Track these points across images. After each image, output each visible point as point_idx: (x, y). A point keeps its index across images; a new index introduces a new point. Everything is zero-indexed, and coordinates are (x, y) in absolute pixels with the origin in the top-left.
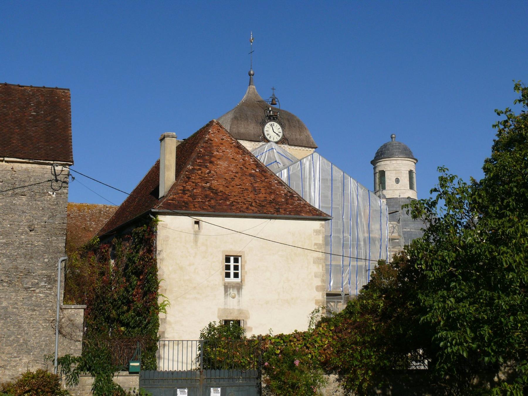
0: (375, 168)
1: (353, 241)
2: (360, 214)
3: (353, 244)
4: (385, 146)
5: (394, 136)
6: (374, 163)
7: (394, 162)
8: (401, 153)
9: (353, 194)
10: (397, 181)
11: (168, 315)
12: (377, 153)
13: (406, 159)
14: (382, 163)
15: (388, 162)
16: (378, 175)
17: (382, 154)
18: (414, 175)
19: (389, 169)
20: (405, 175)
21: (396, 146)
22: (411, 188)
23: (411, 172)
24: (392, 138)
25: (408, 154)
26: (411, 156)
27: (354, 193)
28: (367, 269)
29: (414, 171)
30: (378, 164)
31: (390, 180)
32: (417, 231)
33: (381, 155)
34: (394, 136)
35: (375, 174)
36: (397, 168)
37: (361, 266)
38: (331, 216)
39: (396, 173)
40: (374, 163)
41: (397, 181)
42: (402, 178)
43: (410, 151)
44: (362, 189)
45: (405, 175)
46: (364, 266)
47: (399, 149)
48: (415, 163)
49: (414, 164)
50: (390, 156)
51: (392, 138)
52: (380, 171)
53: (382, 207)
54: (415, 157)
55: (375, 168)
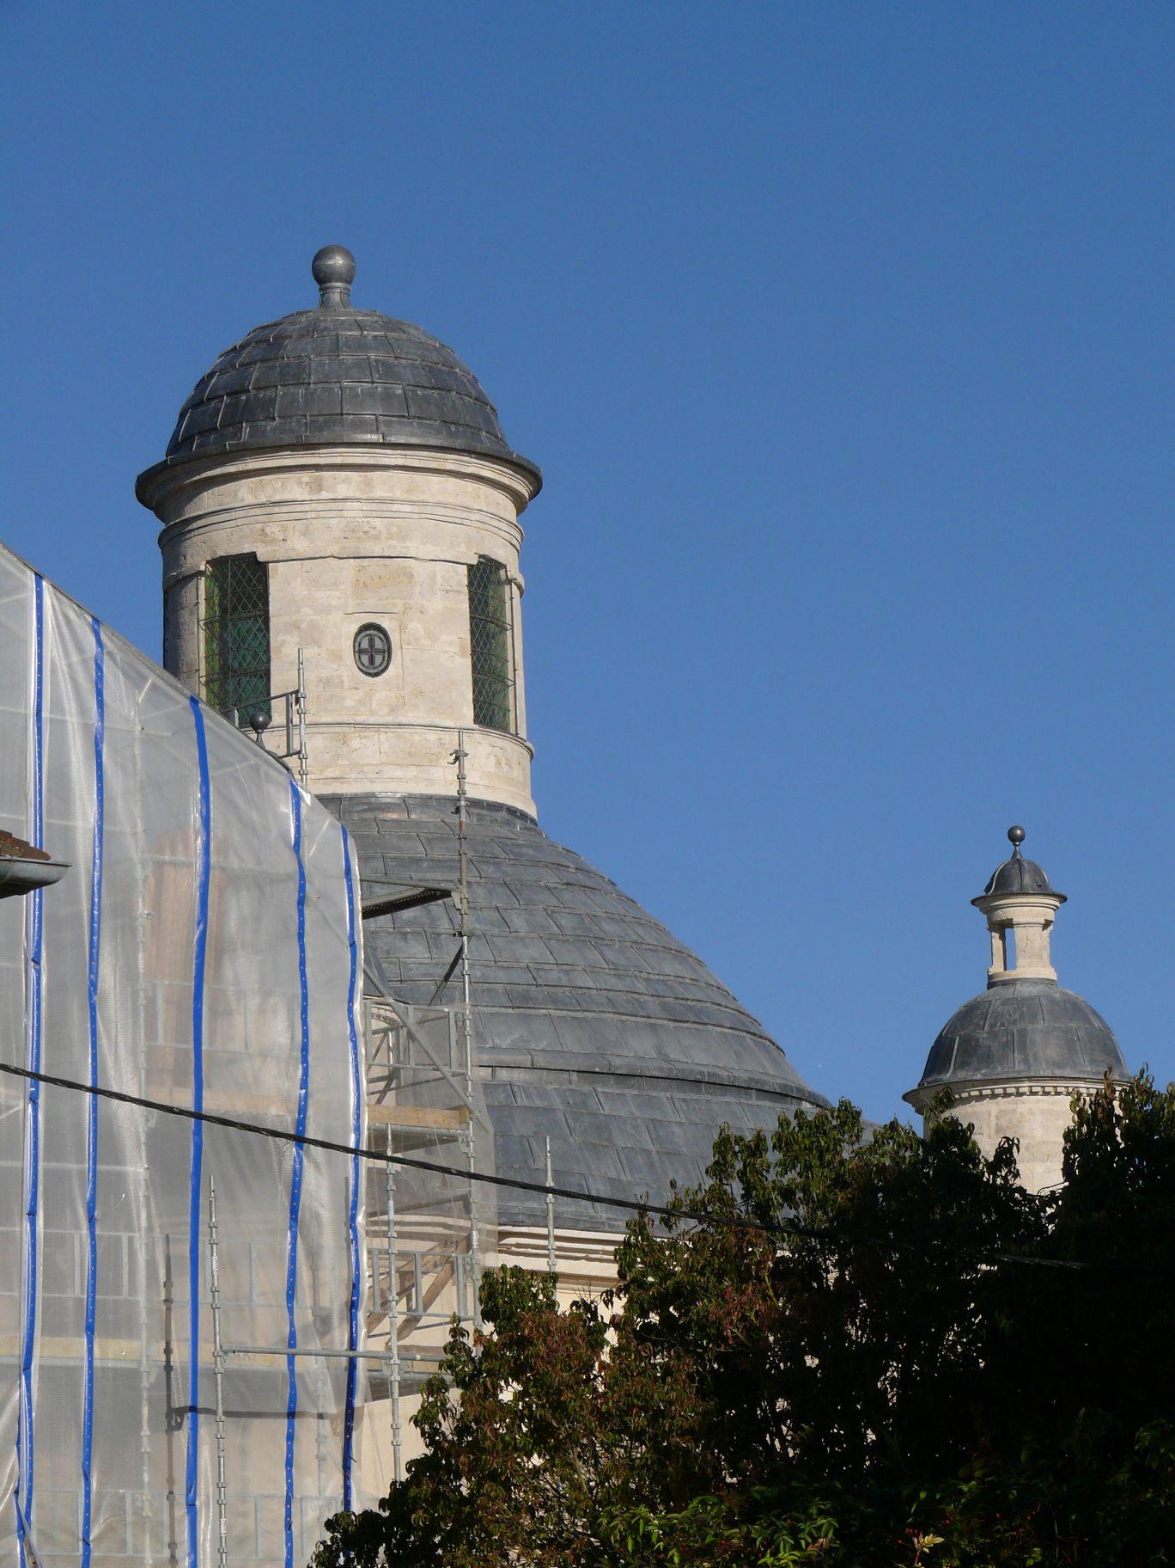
0: (172, 541)
1: (54, 1152)
2: (125, 910)
3: (57, 1180)
4: (267, 343)
5: (338, 261)
6: (166, 490)
7: (345, 485)
8: (409, 409)
9: (60, 725)
10: (373, 649)
11: (652, 1203)
12: (196, 403)
13: (451, 462)
14: (244, 492)
15: (292, 487)
16: (199, 597)
17: (233, 417)
18: (514, 608)
19: (300, 546)
20: (437, 604)
21: (361, 345)
22: (489, 713)
23: (484, 578)
24: (322, 278)
25: (455, 417)
26: (486, 444)
27: (73, 720)
28: (181, 1400)
29: (513, 571)
30: (208, 500)
31: (312, 636)
32: (552, 1084)
33: (234, 419)
34: (338, 261)
35: (174, 587)
36: (373, 546)
37: (130, 1376)
38: (39, 855)
39: (360, 587)
40: (166, 490)
41: (373, 649)
42: (416, 627)
43: (481, 400)
44: (136, 681)
45: (437, 604)
46: (150, 1376)
47: (389, 372)
48: (520, 504)
49: (508, 509)
50: (312, 433)
51: (322, 278)
52: (219, 563)
53: (310, 851)
54: (518, 447)
55: (172, 541)
